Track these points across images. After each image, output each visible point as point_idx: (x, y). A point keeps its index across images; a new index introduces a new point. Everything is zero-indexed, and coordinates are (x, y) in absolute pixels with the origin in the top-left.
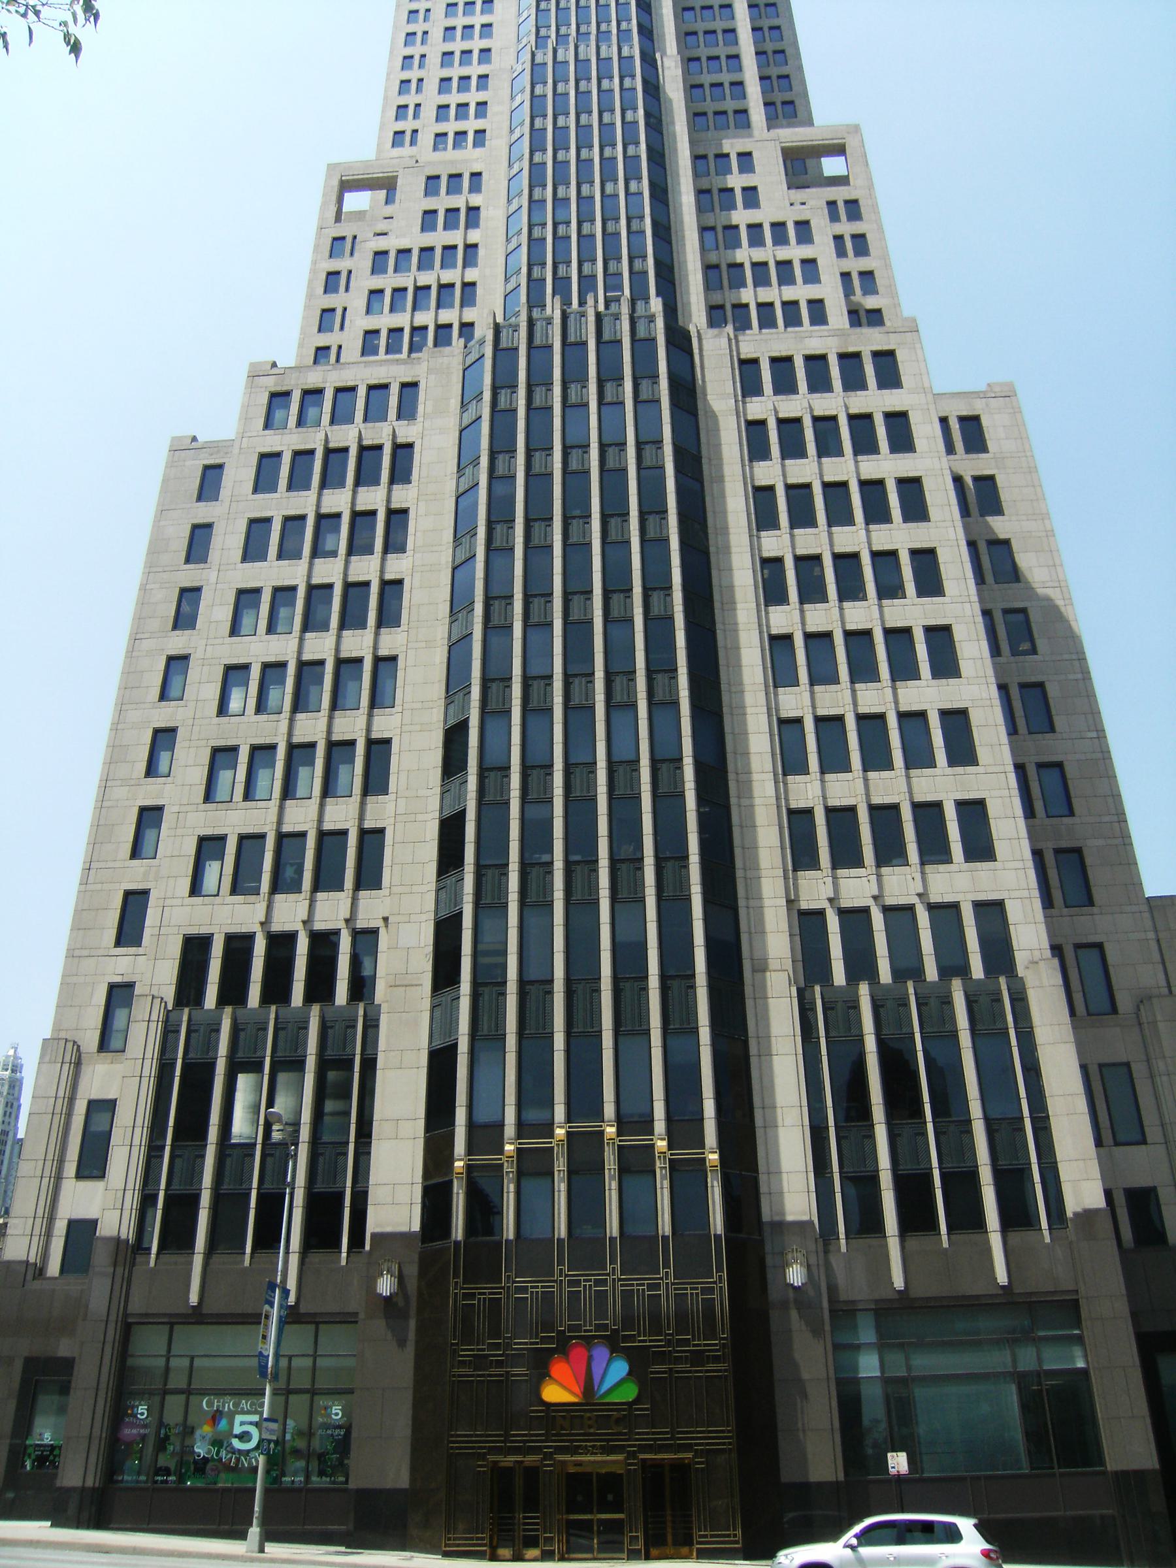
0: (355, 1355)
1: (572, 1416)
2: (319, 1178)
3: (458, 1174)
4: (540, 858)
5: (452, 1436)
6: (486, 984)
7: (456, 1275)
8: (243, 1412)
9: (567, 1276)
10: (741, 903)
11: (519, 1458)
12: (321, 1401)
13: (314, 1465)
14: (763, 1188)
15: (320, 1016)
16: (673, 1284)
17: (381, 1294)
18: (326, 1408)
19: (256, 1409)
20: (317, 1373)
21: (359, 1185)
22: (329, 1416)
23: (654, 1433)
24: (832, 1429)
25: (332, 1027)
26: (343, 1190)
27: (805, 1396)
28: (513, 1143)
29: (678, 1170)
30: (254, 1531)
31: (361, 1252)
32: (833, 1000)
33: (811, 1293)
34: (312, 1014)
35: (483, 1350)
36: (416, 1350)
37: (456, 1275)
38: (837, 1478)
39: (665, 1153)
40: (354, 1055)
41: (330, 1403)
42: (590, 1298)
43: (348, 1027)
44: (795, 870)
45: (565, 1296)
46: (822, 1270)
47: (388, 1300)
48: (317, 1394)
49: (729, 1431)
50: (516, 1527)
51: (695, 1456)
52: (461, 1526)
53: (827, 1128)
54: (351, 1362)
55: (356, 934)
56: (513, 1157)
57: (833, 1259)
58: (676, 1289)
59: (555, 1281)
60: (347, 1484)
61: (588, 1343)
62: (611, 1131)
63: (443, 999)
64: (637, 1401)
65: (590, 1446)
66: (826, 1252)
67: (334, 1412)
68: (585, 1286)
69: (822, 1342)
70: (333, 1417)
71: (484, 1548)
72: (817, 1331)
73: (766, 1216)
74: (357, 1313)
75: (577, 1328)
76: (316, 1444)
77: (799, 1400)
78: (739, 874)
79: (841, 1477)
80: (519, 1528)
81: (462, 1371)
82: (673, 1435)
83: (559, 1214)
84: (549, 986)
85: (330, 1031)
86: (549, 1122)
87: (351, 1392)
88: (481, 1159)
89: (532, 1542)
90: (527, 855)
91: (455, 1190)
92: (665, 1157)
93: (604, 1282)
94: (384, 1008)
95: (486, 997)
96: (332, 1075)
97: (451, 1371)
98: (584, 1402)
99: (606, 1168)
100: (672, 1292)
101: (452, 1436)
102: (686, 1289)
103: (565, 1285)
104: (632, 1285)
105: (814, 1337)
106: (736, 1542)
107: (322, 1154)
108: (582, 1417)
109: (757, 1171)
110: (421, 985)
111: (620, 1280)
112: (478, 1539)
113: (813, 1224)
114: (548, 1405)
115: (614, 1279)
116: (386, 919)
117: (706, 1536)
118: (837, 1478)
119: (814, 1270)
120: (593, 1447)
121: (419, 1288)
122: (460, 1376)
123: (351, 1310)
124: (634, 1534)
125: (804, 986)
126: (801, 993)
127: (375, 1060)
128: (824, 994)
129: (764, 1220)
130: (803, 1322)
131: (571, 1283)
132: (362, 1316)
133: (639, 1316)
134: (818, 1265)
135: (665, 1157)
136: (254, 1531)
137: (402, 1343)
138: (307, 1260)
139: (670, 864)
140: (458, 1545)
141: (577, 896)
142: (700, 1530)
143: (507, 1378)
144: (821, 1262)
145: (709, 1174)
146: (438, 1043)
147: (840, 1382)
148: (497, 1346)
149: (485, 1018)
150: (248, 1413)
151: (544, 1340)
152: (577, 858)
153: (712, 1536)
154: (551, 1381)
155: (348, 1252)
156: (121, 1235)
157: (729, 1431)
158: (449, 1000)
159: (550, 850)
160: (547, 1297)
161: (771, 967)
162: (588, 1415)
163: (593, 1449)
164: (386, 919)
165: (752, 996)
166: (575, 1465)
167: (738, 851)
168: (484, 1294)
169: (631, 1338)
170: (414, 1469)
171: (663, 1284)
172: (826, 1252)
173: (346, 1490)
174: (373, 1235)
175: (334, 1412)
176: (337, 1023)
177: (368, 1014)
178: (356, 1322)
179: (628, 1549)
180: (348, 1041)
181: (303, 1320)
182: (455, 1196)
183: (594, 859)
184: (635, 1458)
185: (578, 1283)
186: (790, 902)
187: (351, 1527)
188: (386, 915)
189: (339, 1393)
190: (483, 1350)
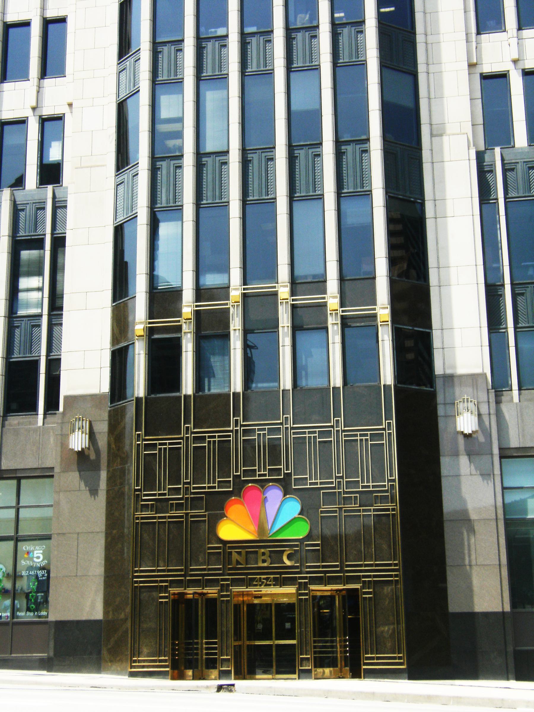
0: (51, 506)
1: (246, 551)
2: (16, 349)
3: (139, 336)
4: (216, 32)
5: (136, 571)
6: (163, 159)
8: (37, 550)
9: (242, 426)
10: (421, 68)
11: (199, 590)
12: (24, 547)
13: (21, 603)
14: (436, 343)
15: (11, 200)
17: (72, 449)
18: (28, 553)
20: (20, 523)
21: (53, 354)
22: (32, 559)
23: (324, 567)
24: (500, 565)
25: (23, 210)
26: (37, 358)
27: (472, 530)
28: (190, 306)
29: (350, 327)
31: (55, 414)
32: (513, 161)
33: (482, 439)
34: (3, 198)
36: (108, 498)
38: (503, 608)
39: (337, 310)
40: (45, 235)
41: (32, 548)
43: (38, 209)
44: (478, 33)
46: (493, 418)
47: (81, 454)
48: (20, 541)
49: (396, 565)
50: (199, 652)
51: (363, 587)
52: (145, 650)
53: (503, 285)
54: (48, 512)
55: (43, 121)
56: (191, 319)
57: (504, 408)
60: (48, 618)
61: (262, 487)
62: (284, 292)
63: (126, 175)
65: (264, 579)
66: (498, 402)
67: (35, 555)
69: (491, 484)
70: (35, 560)
71: (167, 669)
72: (486, 475)
73: (439, 369)
74: (53, 468)
76: (23, 584)
77: (465, 534)
78: (420, 39)
79: (507, 608)
80: (202, 652)
81: (145, 514)
82: (342, 568)
83: (235, 369)
84: (225, 158)
85: (22, 214)
86: (226, 286)
87: (48, 538)
88: (160, 322)
89: (212, 664)
90: (202, 29)
91: (137, 352)
92: (336, 314)
94: (70, 191)
95: (164, 172)
96: (25, 254)
97: (134, 515)
98: (258, 539)
99: (280, 325)
101: (136, 571)
104: (305, 433)
105: (483, 480)
107: (18, 327)
108: (256, 552)
109: (430, 327)
110: (106, 165)
111: (292, 428)
112: (161, 661)
113: (486, 377)
114: (225, 543)
116: (70, 105)
117: (373, 658)
118: (503, 608)
119: (486, 419)
120: (267, 579)
121: (109, 445)
122: (143, 518)
123: (48, 464)
125: (484, 149)
126: (480, 156)
127: (64, 238)
128: (504, 155)
129: (436, 374)
130: (473, 467)
131: (245, 432)
132: (57, 470)
134: (489, 414)
135: (336, 314)
137: (94, 492)
138: (7, 423)
139: (346, 31)
140: (143, 667)
141: (252, 67)
143: (187, 519)
144: (493, 411)
145: (380, 328)
146: (122, 218)
147: (508, 523)
149: (164, 191)
152: (253, 29)
153: (378, 658)
154: (228, 521)
155: (45, 414)
157: (396, 565)
158: (131, 176)
159: (225, 23)
161: (448, 131)
162: (263, 550)
163: (267, 581)
164: (70, 105)
165: (430, 160)
167: (419, 17)
168: (165, 444)
170: (107, 603)
171: (334, 431)
172: (498, 402)
173: (46, 623)
174: (66, 398)
175: (35, 555)
176: (28, 206)
177: (57, 196)
178: (52, 476)
179: (299, 670)
180: (36, 223)
181: (5, 476)
182: (137, 357)
183: (270, 29)
184: (306, 588)
186: (471, 66)
187: (52, 654)
188: (70, 101)
189: (39, 539)
190: (165, 494)
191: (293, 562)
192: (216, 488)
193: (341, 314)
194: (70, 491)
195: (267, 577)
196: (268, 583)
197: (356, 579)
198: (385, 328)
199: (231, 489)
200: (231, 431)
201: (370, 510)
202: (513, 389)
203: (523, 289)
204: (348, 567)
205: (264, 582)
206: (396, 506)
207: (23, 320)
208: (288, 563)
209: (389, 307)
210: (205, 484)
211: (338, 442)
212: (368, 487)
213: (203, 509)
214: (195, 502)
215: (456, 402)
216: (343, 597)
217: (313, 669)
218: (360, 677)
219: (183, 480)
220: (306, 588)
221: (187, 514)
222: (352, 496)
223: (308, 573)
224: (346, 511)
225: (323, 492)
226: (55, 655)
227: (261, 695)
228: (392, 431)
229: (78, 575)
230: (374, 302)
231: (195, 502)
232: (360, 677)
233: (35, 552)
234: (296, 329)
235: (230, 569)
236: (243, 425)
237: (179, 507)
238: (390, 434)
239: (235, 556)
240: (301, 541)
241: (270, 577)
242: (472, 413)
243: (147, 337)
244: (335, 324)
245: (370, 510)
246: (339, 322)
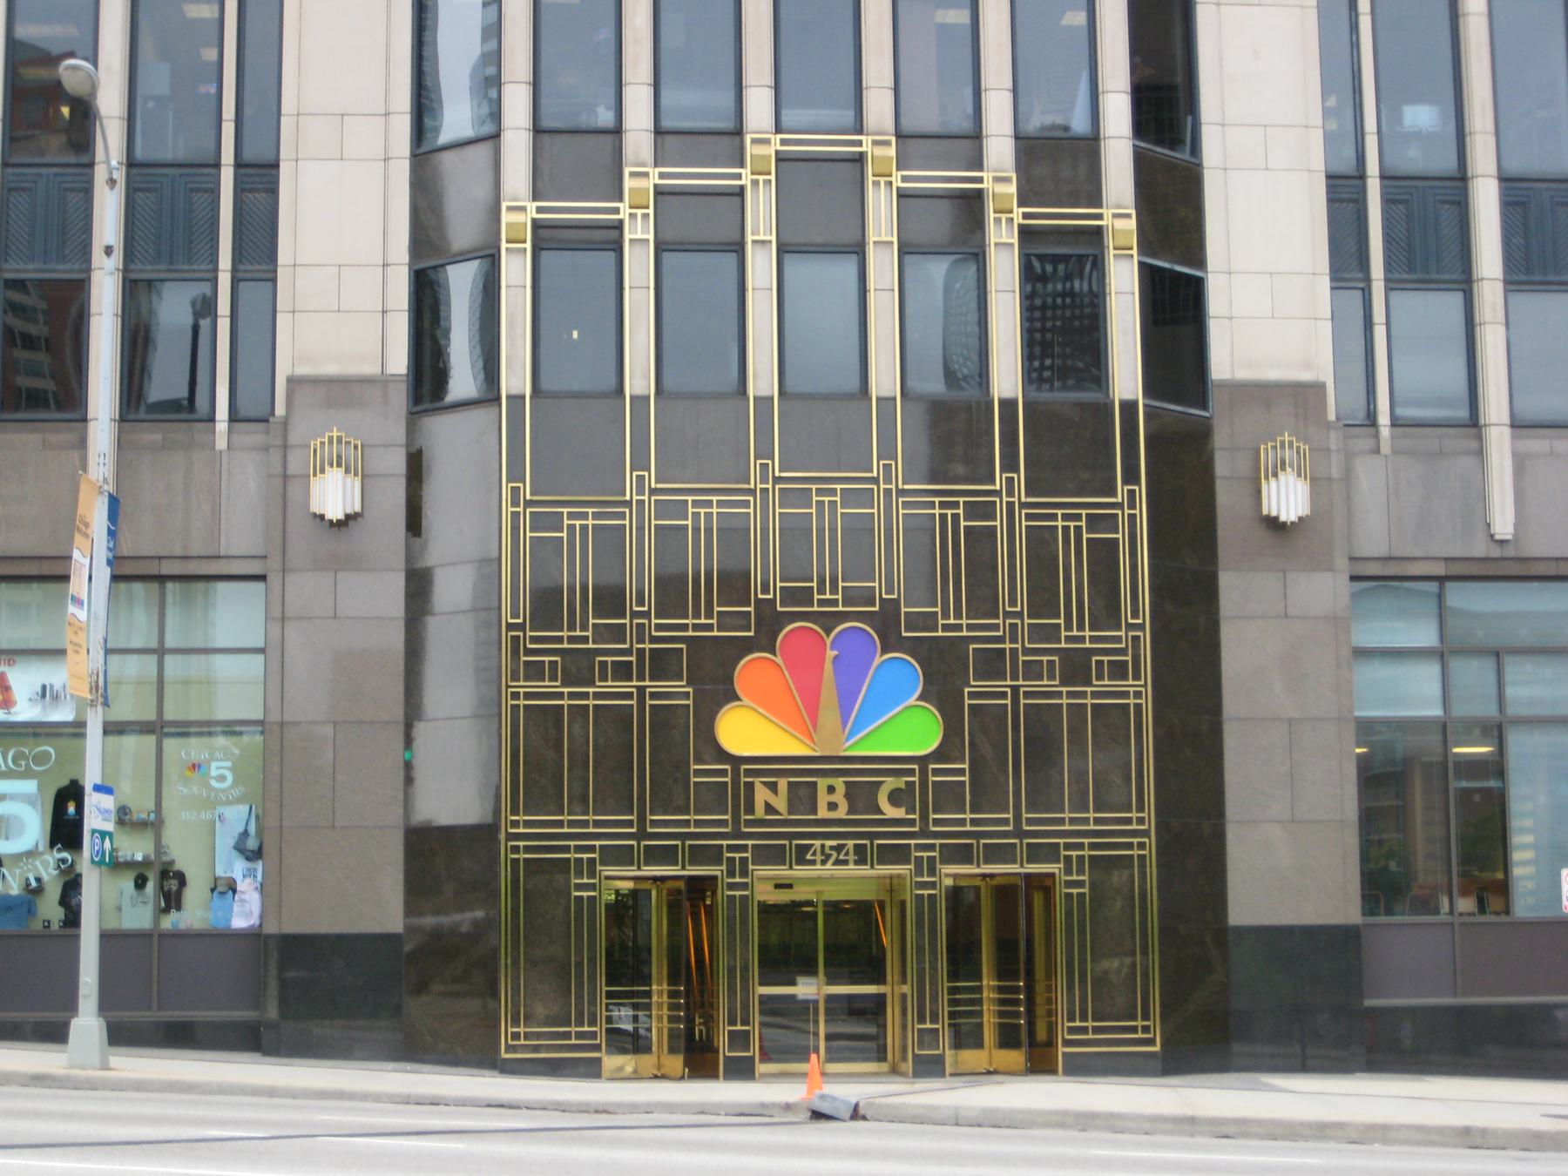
8: (217, 760)
9: (528, 504)
16: (1023, 505)
19: (27, 765)
26: (82, 276)
30: (87, 1024)
35: (709, 627)
37: (640, 463)
41: (205, 755)
42: (833, 530)
45: (775, 525)
58: (1029, 517)
59: (752, 492)
64: (939, 754)
65: (832, 848)
68: (696, 516)
75: (805, 596)
93: (866, 498)
106: (1151, 1042)
111: (901, 493)
115: (888, 492)
120: (839, 848)
124: (928, 1026)
129: (1213, 377)
136: (87, 1024)
140: (536, 1049)
148: (618, 633)
150: (221, 760)
151: (725, 621)
160: (734, 533)
166: (778, 886)
169: (928, 621)
175: (214, 773)
179: (915, 1056)
185: (555, 522)
191: (903, 810)
194: (310, 618)
195: (838, 845)
196: (841, 857)
197: (1051, 853)
198: (1125, 264)
199: (751, 634)
200: (752, 492)
201: (585, 696)
202: (217, 418)
203: (1404, 191)
205: (831, 855)
206: (1145, 685)
207: (167, 175)
208: (891, 812)
209: (1133, 212)
210: (687, 618)
211: (640, 529)
213: (682, 680)
214: (661, 664)
216: (671, 892)
218: (714, 1076)
219: (1004, 604)
221: (641, 690)
222: (544, 662)
225: (973, 649)
226: (283, 1016)
227: (566, 1114)
229: (336, 825)
230: (1095, 198)
231: (661, 664)
233: (214, 765)
234: (906, 250)
235: (749, 823)
236: (780, 477)
237: (623, 671)
238: (1132, 517)
239: (762, 795)
240: (923, 760)
242: (347, 471)
245: (585, 696)
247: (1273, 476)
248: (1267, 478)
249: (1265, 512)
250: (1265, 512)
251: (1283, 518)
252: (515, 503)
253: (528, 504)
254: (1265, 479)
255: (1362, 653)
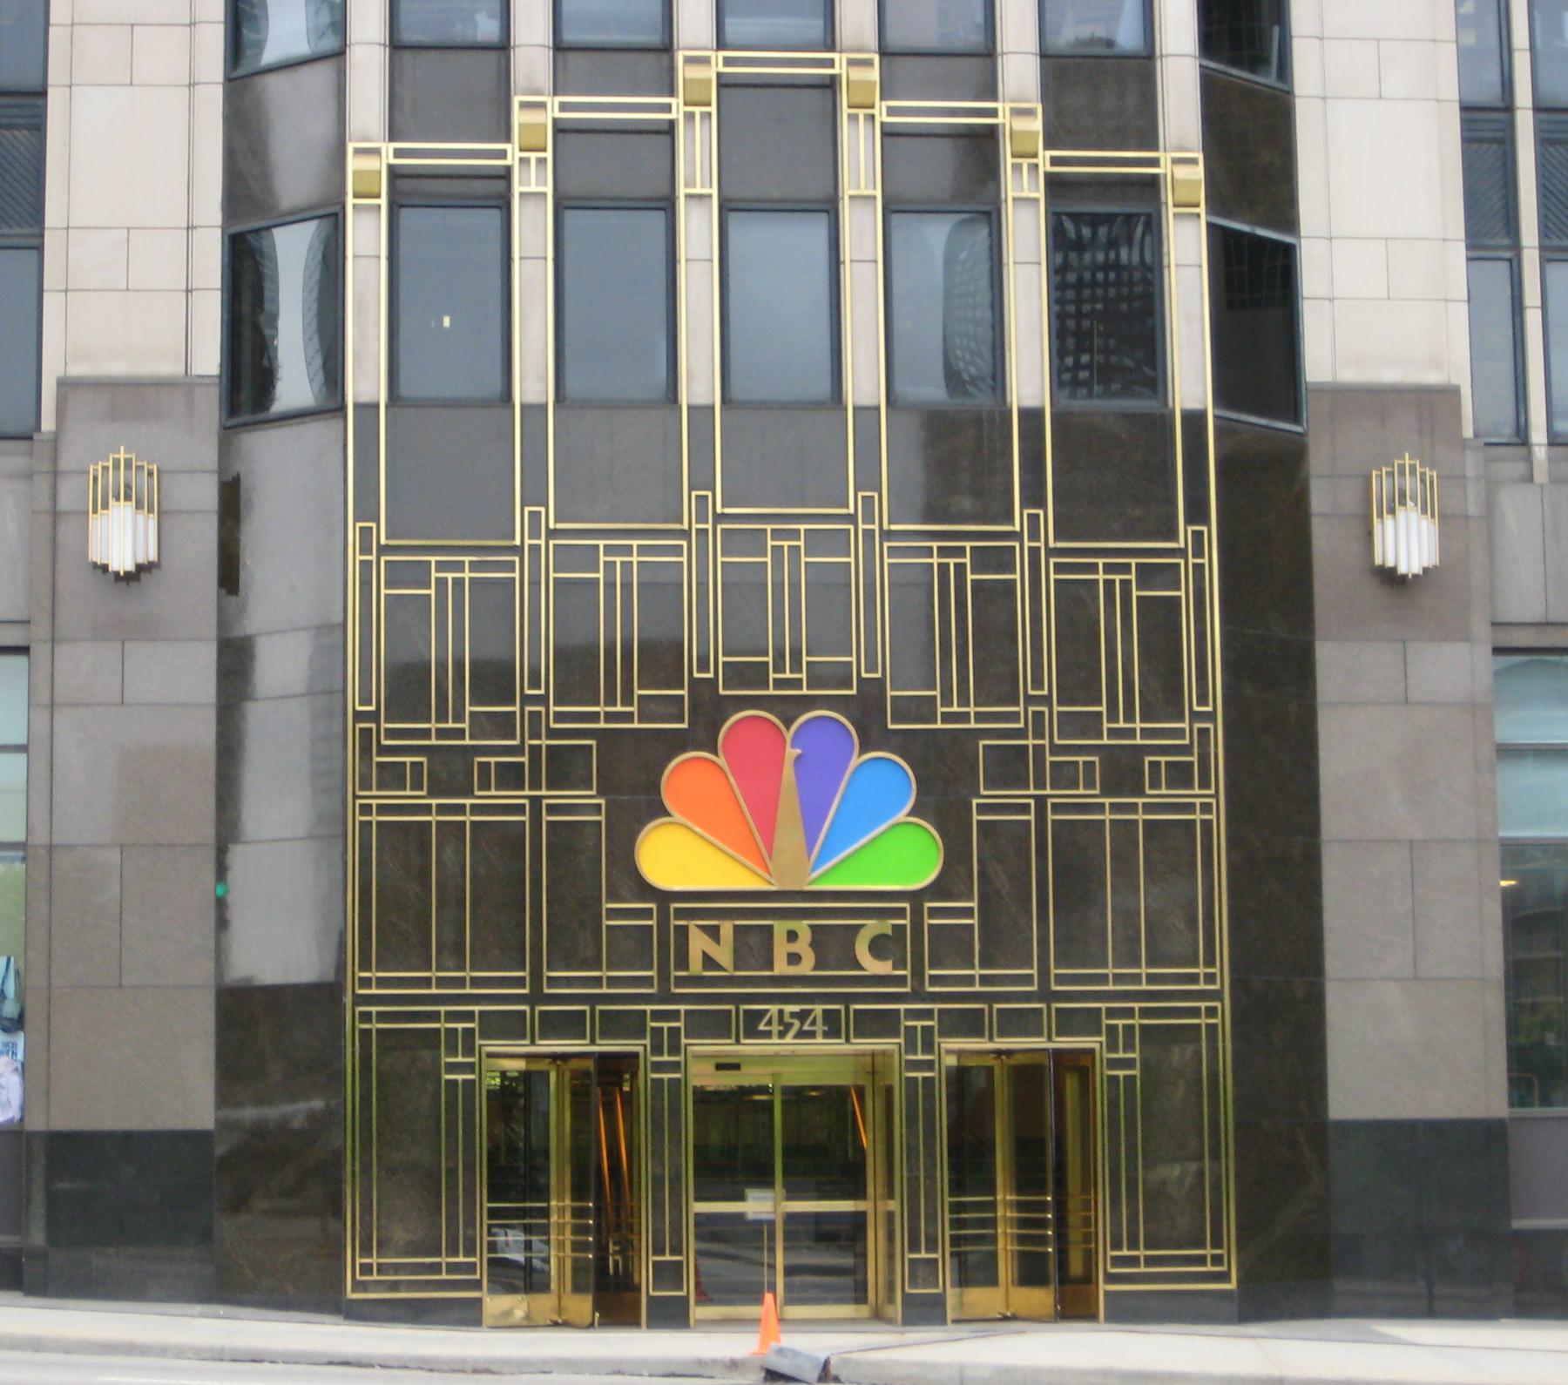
7: (535, 494)
16: (1051, 552)
42: (795, 586)
45: (714, 581)
58: (1060, 568)
59: (686, 534)
64: (938, 889)
65: (793, 1015)
75: (756, 675)
93: (839, 542)
100: (1050, 577)
102: (1093, 568)
103: (548, 559)
106: (1224, 1277)
111: (887, 535)
124: (923, 1255)
129: (1308, 379)
131: (565, 558)
133: (442, 666)
140: (394, 1286)
142: (1117, 1245)
151: (649, 709)
156: (199, 230)
169: (923, 710)
179: (905, 1296)
191: (890, 963)
192: (632, 721)
193: (1050, 169)
195: (802, 1011)
196: (806, 1027)
197: (1087, 1022)
198: (367, 220)
199: (685, 726)
200: (686, 534)
204: (684, 987)
206: (1216, 795)
208: (874, 966)
209: (1200, 156)
210: (598, 704)
211: (535, 584)
212: (1130, 733)
215: (92, 467)
217: (952, 1294)
220: (928, 1046)
223: (935, 998)
224: (1057, 808)
225: (985, 747)
228: (1205, 561)
232: (1089, 1315)
234: (894, 207)
235: (681, 982)
237: (511, 776)
238: (1199, 568)
239: (698, 943)
240: (915, 897)
241: (811, 1011)
243: (1003, 197)
244: (700, 197)
245: (460, 809)
246: (1040, 194)
247: (1388, 513)
248: (1380, 515)
249: (1378, 561)
250: (1378, 561)
251: (1402, 569)
252: (365, 549)
253: (383, 550)
254: (1378, 516)
255: (1510, 752)
